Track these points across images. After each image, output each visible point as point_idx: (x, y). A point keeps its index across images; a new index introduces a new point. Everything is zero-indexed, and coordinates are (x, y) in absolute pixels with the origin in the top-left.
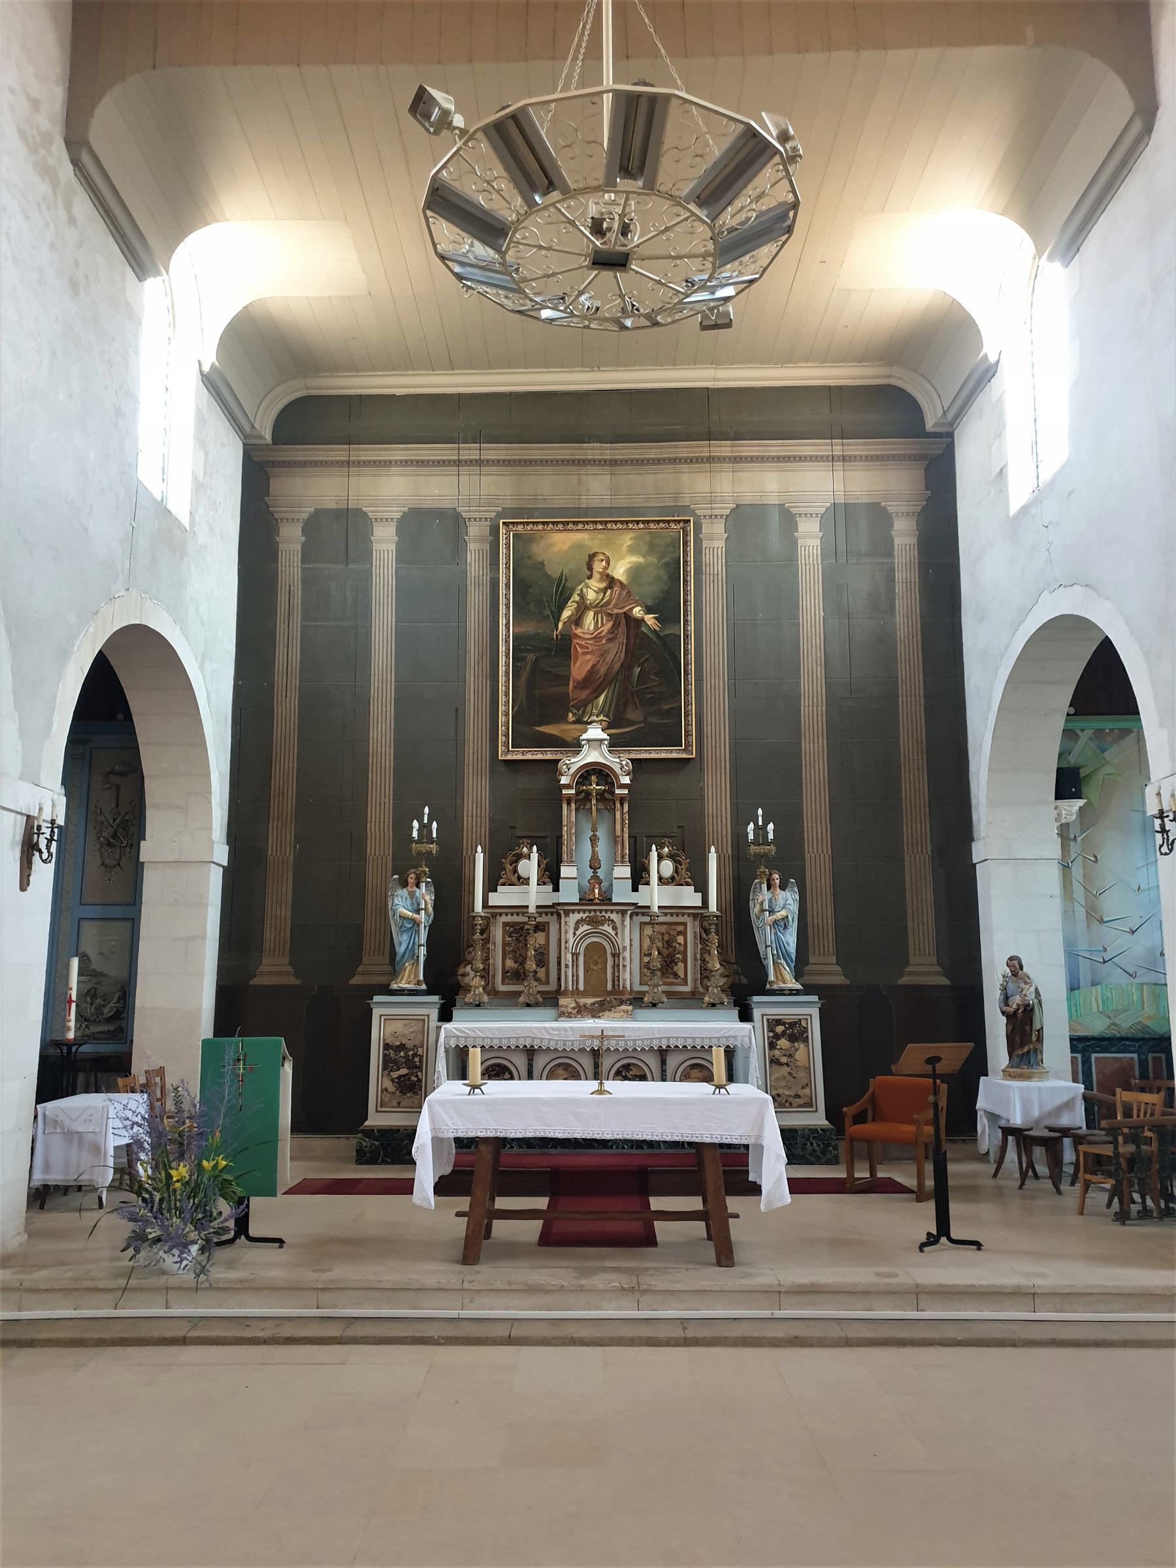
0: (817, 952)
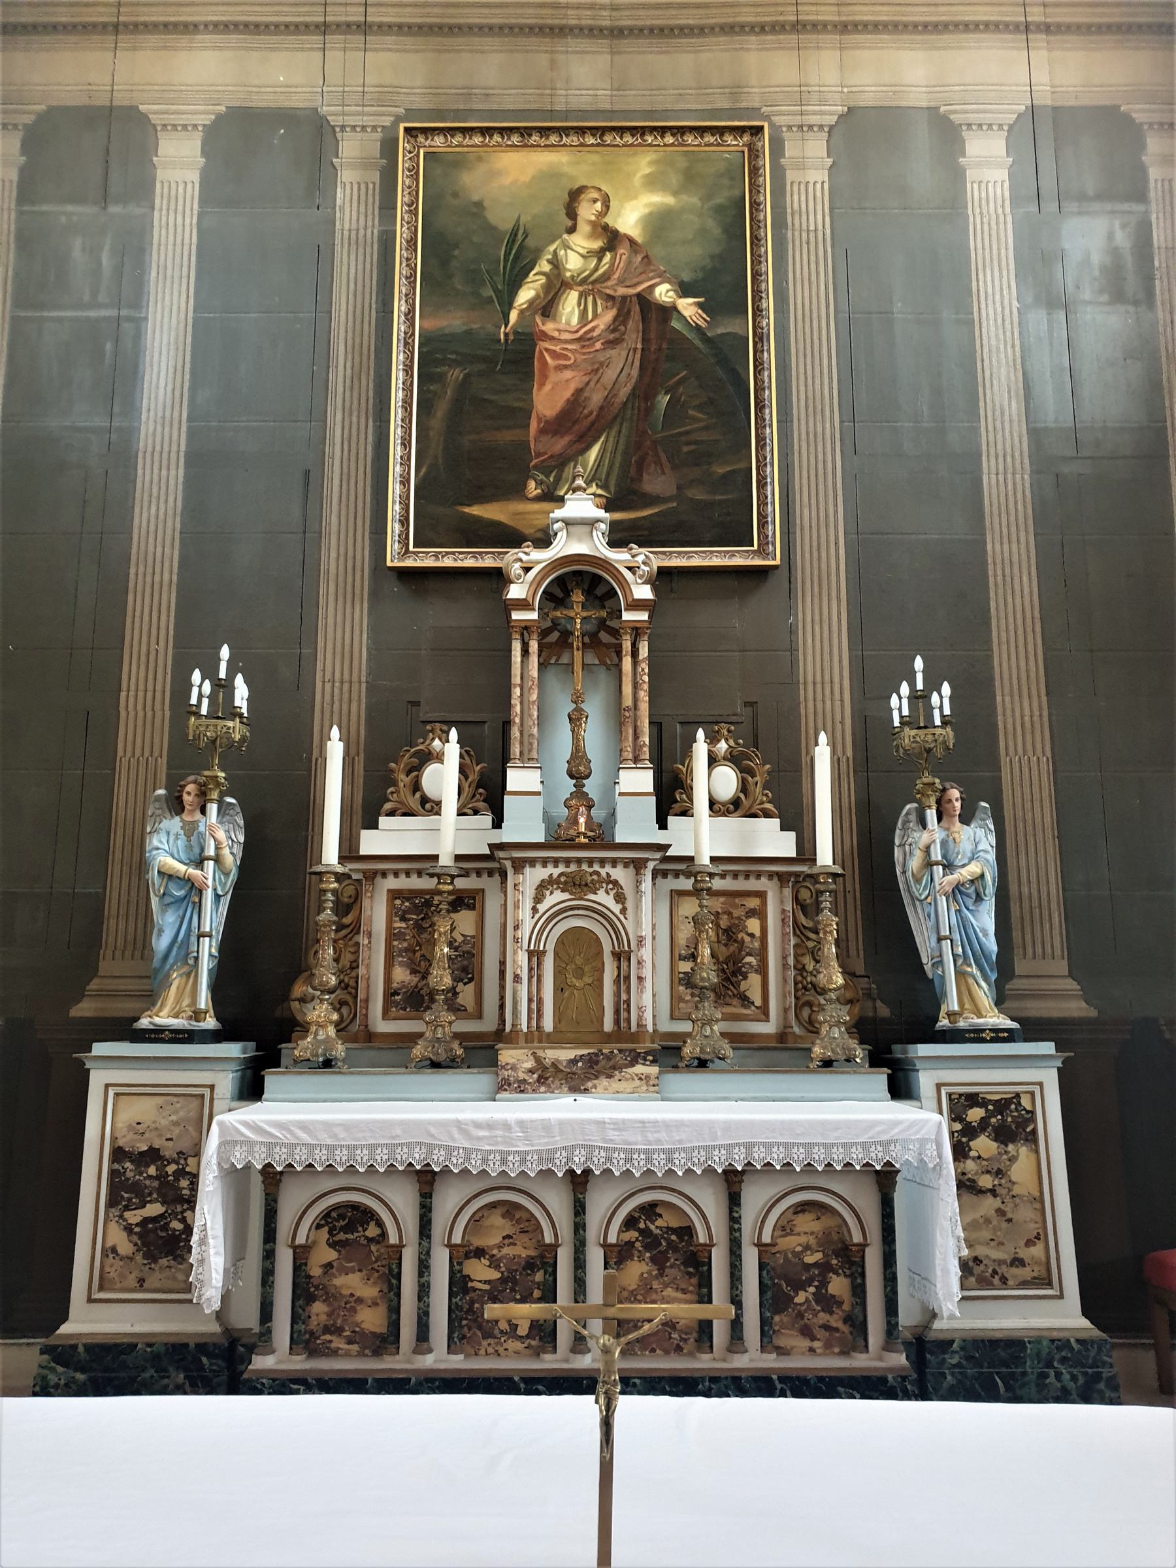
0: (1030, 950)
